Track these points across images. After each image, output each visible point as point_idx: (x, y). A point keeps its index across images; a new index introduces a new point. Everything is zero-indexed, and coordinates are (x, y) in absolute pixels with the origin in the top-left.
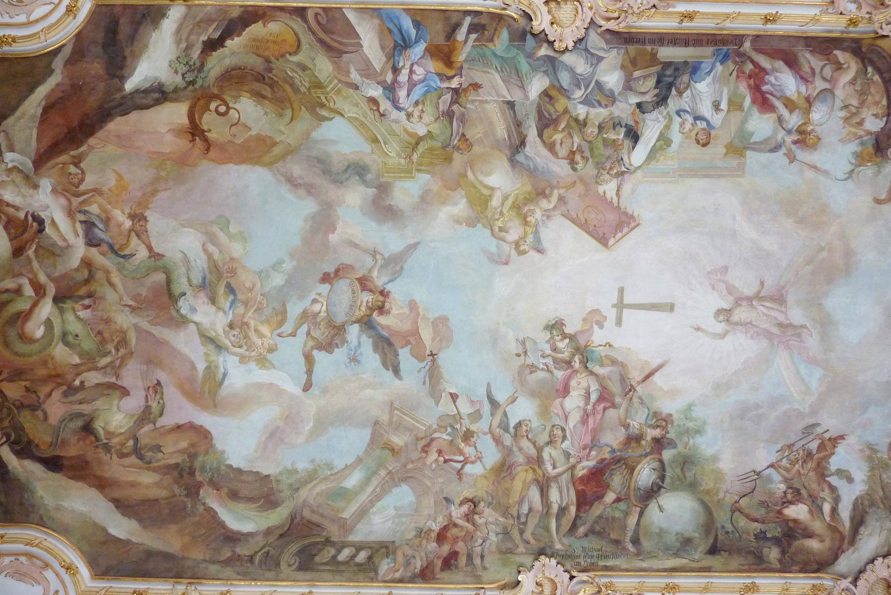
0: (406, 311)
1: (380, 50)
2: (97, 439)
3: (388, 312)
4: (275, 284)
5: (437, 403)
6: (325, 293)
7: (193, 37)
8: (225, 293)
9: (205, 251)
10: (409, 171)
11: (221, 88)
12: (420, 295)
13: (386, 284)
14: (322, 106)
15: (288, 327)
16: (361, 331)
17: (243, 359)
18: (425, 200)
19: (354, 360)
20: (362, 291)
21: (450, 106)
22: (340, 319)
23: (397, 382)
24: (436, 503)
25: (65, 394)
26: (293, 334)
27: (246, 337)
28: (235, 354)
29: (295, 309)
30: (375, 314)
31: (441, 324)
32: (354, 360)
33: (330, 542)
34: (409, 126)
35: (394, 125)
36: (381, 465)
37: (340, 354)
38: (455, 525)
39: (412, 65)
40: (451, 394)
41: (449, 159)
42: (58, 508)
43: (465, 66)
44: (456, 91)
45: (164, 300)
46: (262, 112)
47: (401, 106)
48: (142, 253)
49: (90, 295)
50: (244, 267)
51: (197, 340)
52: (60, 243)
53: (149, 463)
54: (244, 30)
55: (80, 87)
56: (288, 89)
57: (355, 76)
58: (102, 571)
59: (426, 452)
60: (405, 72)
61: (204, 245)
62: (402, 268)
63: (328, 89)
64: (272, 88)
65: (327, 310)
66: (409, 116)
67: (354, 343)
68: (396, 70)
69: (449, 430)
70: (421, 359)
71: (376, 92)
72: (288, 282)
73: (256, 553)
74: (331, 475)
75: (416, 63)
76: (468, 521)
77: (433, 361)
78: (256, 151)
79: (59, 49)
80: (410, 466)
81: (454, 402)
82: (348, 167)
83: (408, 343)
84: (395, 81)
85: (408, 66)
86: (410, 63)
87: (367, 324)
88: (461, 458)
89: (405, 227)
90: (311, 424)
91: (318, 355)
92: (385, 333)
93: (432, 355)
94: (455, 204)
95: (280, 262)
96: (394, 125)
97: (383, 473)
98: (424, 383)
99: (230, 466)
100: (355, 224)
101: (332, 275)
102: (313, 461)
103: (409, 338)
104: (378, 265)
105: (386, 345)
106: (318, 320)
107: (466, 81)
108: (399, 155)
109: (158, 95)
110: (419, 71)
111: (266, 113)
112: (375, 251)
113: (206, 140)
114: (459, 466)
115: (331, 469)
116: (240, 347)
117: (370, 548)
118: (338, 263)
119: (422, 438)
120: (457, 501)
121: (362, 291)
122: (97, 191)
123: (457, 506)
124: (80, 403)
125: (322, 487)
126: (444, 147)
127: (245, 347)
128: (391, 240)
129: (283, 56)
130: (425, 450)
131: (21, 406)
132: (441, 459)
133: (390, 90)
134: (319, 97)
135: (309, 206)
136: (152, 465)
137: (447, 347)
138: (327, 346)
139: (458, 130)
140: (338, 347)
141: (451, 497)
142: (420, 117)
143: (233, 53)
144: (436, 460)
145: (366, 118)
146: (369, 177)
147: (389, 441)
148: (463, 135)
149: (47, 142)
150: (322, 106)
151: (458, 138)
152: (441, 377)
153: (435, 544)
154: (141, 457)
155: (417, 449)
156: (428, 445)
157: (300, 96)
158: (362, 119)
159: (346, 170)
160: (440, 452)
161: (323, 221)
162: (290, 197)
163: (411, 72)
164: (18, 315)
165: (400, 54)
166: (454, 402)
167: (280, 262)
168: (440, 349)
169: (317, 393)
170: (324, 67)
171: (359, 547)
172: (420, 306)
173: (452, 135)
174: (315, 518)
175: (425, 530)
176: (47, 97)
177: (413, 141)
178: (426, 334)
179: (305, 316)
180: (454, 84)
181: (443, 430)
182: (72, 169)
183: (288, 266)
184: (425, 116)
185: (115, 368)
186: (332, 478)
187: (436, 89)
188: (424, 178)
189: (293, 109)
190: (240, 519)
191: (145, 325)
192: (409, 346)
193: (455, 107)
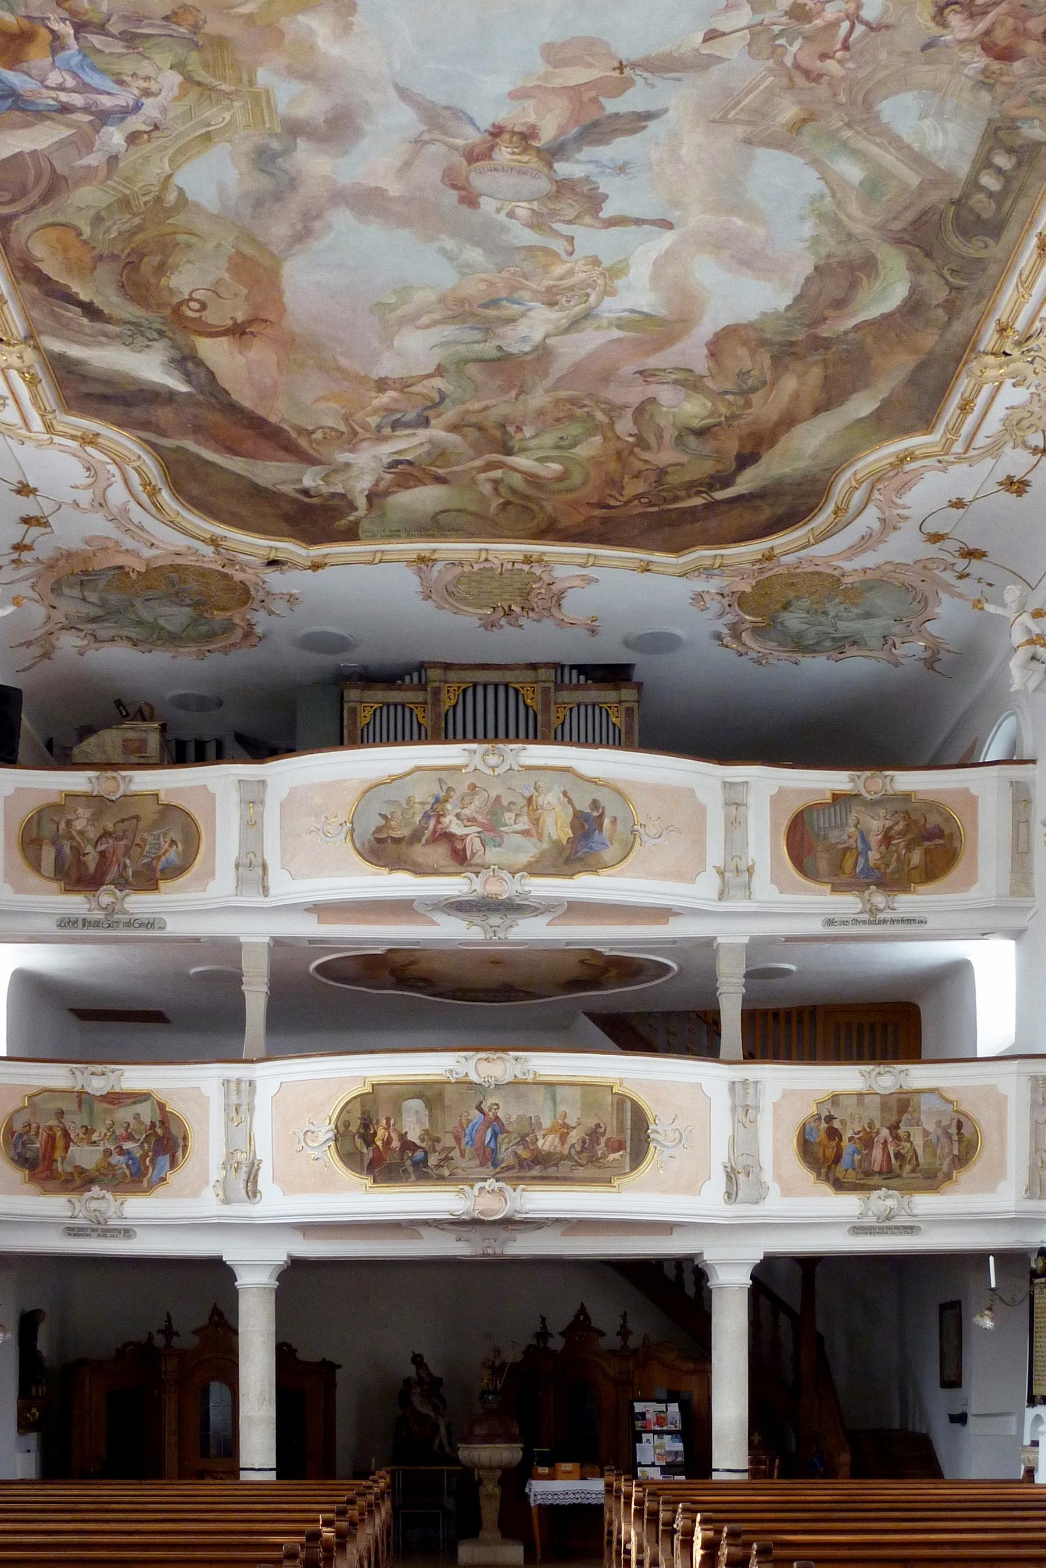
0: (530, 104)
1: (31, 130)
2: (719, 424)
3: (533, 127)
4: (481, 259)
5: (720, 60)
6: (497, 204)
7: (88, 331)
8: (498, 309)
9: (428, 327)
10: (256, 98)
11: (160, 306)
12: (504, 84)
13: (478, 129)
14: (159, 199)
15: (558, 246)
16: (567, 160)
17: (609, 292)
18: (308, 70)
19: (622, 169)
20: (490, 158)
21: (113, 36)
22: (544, 185)
23: (671, 112)
24: (928, 63)
25: (647, 447)
26: (571, 240)
27: (571, 288)
28: (599, 303)
29: (527, 237)
30: (535, 143)
31: (555, 55)
32: (622, 169)
33: (959, 200)
34: (167, 96)
35: (171, 114)
36: (832, 135)
37: (605, 185)
38: (987, 33)
39: (47, 87)
40: (705, 40)
41: (220, 42)
42: (814, 457)
43: (22, 11)
44: (80, 28)
45: (508, 369)
46: (189, 266)
47: (131, 103)
48: (438, 382)
49: (502, 426)
50: (453, 290)
51: (573, 336)
52: (426, 448)
53: (764, 383)
54: (57, 282)
55: (194, 426)
56: (140, 237)
57: (93, 160)
58: (926, 421)
59: (820, 76)
60: (63, 97)
61: (419, 328)
62: (448, 108)
63: (128, 192)
64: (143, 256)
65: (530, 201)
66: (147, 93)
67: (591, 168)
68: (65, 109)
69: (781, 41)
70: (630, 83)
71: (115, 137)
72: (477, 244)
73: (947, 282)
74: (834, 196)
75: (42, 82)
76: (985, 13)
77: (633, 66)
78: (257, 272)
79: (146, 441)
80: (843, 98)
81: (724, 34)
82: (262, 170)
83: (594, 100)
84: (86, 109)
85: (53, 94)
86: (44, 91)
87: (555, 152)
88: (846, 25)
89: (367, 103)
90: (734, 219)
91: (608, 211)
92: (573, 131)
93: (621, 67)
94: (311, 32)
95: (443, 251)
96: (171, 114)
97: (847, 133)
98: (679, 80)
99: (789, 308)
100: (375, 158)
101: (463, 193)
102: (802, 218)
103: (585, 99)
104: (443, 137)
105: (597, 130)
106: (545, 210)
107: (54, 12)
108: (228, 108)
109: (186, 361)
110: (54, 78)
111: (189, 262)
112: (416, 142)
113: (250, 322)
114: (860, 29)
115: (822, 197)
116: (588, 295)
117: (991, 150)
118: (442, 186)
119: (791, 79)
120: (935, 30)
121: (490, 158)
122: (346, 418)
123: (945, 32)
124: (662, 437)
125: (854, 208)
126: (197, 46)
127: (589, 290)
128: (391, 126)
129: (85, 242)
130: (813, 76)
131: (659, 482)
132: (839, 55)
133: (103, 117)
134: (146, 203)
135: (342, 219)
136: (768, 378)
137: (606, 45)
138: (594, 201)
139: (158, 26)
140: (598, 188)
141: (923, 39)
142: (147, 78)
143: (98, 292)
144: (839, 62)
145: (166, 148)
146: (275, 145)
147: (784, 125)
148: (166, 18)
149: (282, 454)
150: (159, 199)
151: (174, 26)
152: (670, 54)
153: (1017, 64)
154: (754, 390)
155: (811, 89)
156: (807, 73)
157: (31, 371)
158: (171, 152)
159: (270, 174)
160: (824, 56)
161: (368, 202)
162: (328, 239)
163: (61, 88)
164: (528, 482)
165: (33, 103)
166: (724, 34)
167: (443, 251)
168: (612, 56)
169: (677, 213)
170: (88, 197)
171: (984, 162)
172: (520, 84)
173: (170, 36)
174: (910, 216)
175: (981, 77)
176: (216, 451)
177: (195, 91)
178: (577, 76)
179: (538, 223)
180: (67, 29)
181: (779, 50)
182: (318, 435)
183: (450, 244)
184: (142, 73)
185: (613, 410)
186: (839, 195)
187: (84, 56)
188: (263, 76)
189: (175, 233)
190: (890, 292)
191: (548, 383)
192: (601, 99)
193: (114, 28)
